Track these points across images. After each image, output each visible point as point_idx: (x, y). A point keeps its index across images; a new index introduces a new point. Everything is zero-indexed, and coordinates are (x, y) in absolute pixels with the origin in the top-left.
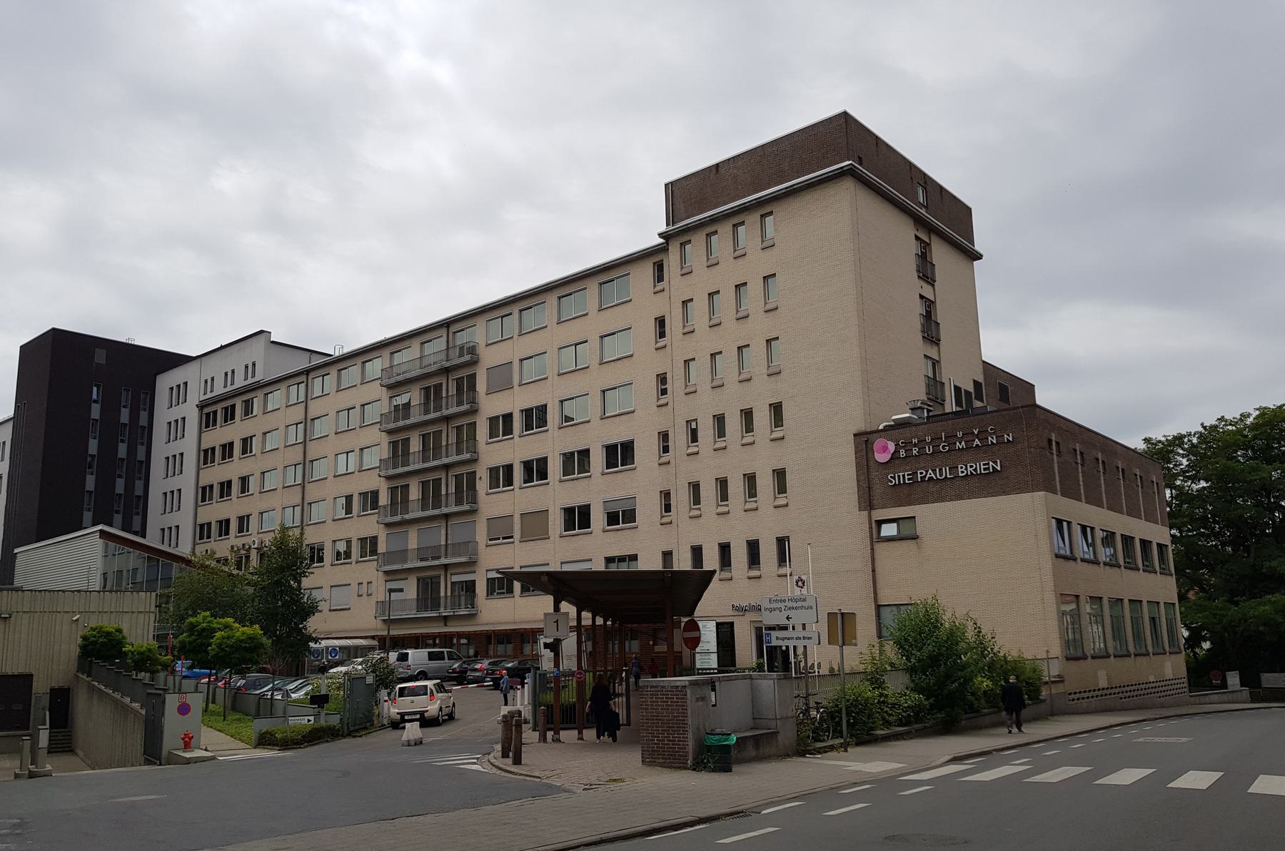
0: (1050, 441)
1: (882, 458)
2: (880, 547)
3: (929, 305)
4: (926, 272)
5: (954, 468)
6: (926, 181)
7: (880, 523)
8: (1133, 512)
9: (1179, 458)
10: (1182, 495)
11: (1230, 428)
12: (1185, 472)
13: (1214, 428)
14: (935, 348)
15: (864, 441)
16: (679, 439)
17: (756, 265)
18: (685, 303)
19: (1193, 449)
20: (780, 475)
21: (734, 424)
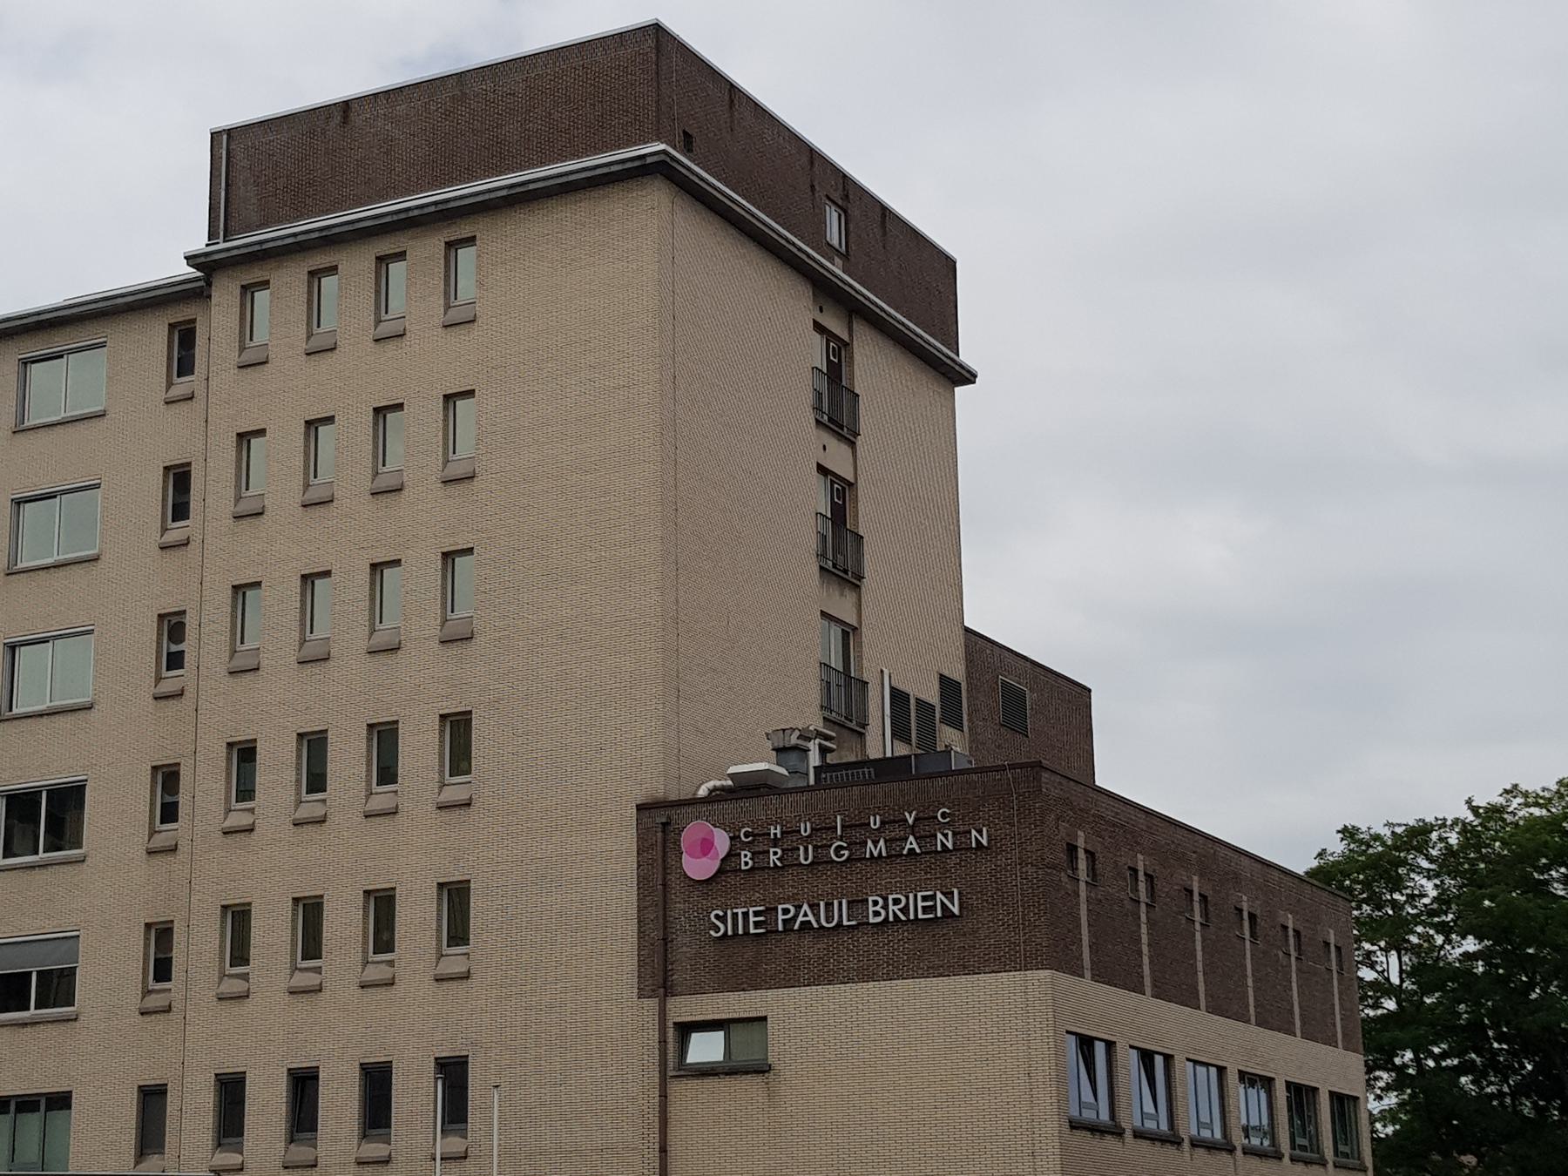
0: (1072, 849)
1: (699, 867)
2: (681, 1091)
3: (842, 491)
4: (837, 413)
5: (857, 903)
6: (848, 193)
7: (686, 1030)
8: (1274, 1018)
9: (1421, 881)
10: (1427, 971)
11: (1536, 812)
12: (1432, 913)
13: (1495, 811)
14: (850, 597)
15: (660, 822)
16: (206, 787)
17: (426, 364)
18: (244, 438)
19: (1449, 862)
20: (456, 896)
21: (349, 761)
